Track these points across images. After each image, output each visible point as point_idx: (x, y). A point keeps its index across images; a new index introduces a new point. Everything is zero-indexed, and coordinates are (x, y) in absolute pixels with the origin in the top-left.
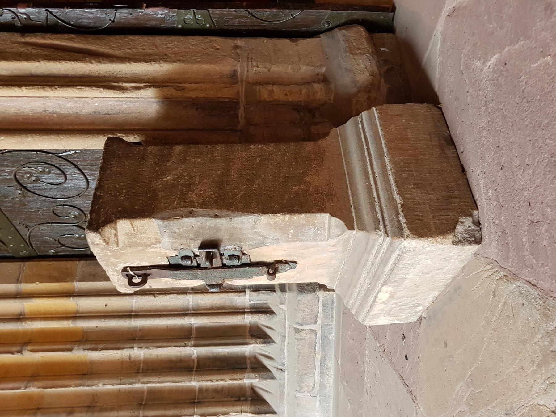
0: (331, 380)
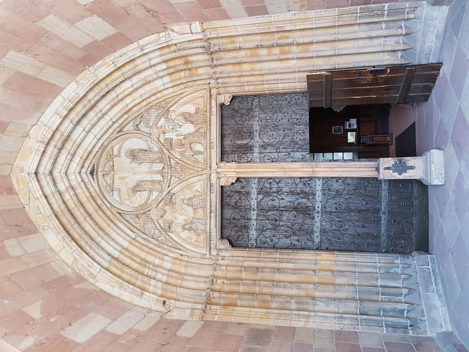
0: (441, 288)
